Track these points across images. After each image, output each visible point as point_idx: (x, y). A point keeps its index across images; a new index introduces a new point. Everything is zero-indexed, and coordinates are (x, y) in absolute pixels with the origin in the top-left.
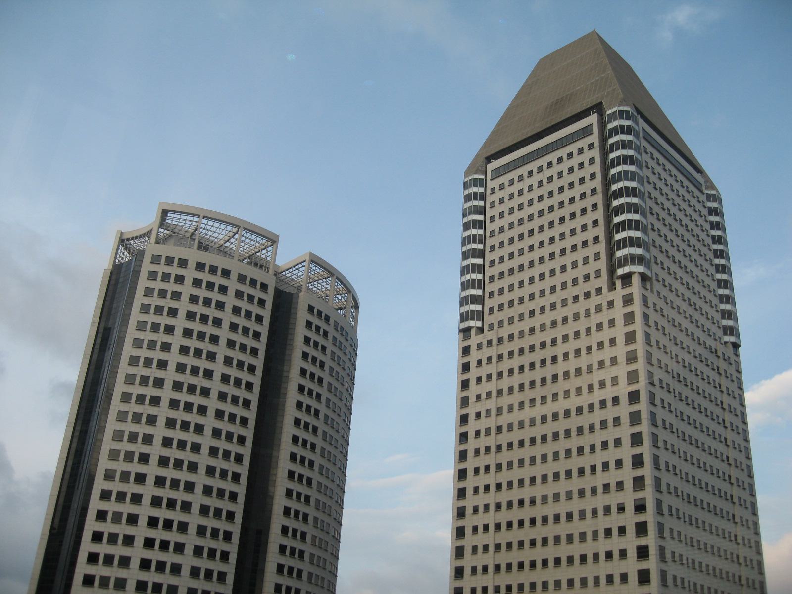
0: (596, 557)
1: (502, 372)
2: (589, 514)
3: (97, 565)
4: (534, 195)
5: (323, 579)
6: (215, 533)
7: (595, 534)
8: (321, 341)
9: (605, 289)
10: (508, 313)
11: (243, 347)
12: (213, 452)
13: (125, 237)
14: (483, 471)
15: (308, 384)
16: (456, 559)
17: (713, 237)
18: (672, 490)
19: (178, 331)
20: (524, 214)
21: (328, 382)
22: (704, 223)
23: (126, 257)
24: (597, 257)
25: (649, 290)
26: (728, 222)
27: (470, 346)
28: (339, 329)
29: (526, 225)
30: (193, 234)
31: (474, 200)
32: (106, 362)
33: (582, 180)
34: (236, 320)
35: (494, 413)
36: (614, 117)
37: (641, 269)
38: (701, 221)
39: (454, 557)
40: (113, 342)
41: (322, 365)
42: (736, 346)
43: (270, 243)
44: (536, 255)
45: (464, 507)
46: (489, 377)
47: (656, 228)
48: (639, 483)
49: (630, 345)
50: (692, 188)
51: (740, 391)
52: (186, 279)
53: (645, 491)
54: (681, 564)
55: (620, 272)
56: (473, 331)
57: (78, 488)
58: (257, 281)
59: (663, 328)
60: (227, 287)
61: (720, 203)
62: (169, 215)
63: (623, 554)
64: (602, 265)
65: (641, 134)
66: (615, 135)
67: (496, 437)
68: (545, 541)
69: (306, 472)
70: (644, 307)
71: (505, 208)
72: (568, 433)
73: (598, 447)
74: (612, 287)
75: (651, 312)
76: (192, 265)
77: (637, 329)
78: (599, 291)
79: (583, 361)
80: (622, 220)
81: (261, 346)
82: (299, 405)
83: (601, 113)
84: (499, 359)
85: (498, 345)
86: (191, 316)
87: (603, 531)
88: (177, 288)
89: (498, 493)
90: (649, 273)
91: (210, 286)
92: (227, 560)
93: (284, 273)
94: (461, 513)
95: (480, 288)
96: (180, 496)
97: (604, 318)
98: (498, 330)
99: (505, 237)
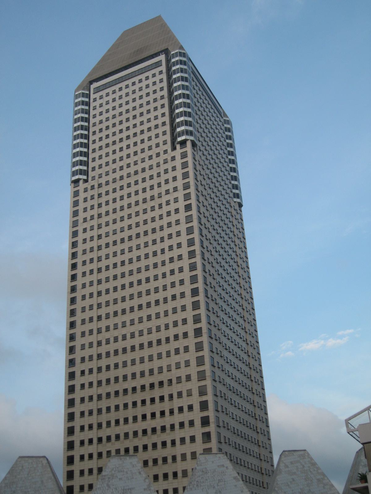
4: (124, 153)
9: (169, 150)
16: (67, 480)
25: (196, 152)
35: (95, 332)
37: (192, 138)
42: (240, 205)
49: (199, 338)
51: (254, 321)
53: (190, 189)
54: (219, 342)
55: (179, 139)
56: (81, 182)
64: (168, 137)
70: (207, 311)
74: (174, 148)
77: (204, 341)
78: (165, 152)
79: (168, 420)
95: (86, 157)
98: (98, 180)
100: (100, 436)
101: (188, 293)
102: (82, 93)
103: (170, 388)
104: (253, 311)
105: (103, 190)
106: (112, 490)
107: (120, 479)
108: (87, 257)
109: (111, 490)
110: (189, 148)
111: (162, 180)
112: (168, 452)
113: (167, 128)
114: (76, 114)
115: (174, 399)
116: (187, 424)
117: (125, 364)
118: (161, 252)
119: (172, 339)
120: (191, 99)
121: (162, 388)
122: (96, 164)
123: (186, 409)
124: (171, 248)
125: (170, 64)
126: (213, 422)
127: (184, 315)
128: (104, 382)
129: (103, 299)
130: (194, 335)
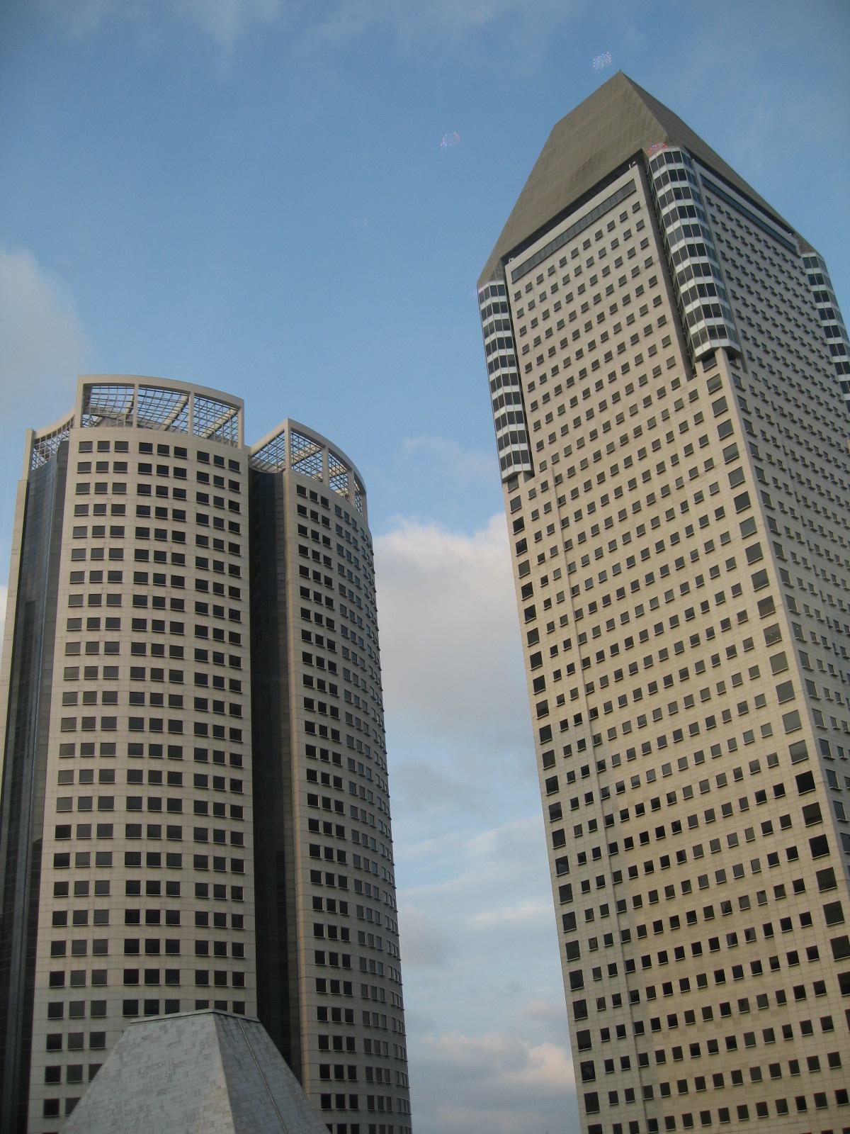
0: (781, 997)
1: (588, 658)
2: (748, 870)
3: (59, 1084)
5: (388, 1071)
6: (220, 949)
7: (756, 865)
8: (327, 656)
9: (683, 379)
11: (218, 658)
12: (200, 835)
13: (39, 436)
14: (584, 803)
15: (318, 719)
17: (827, 329)
19: (122, 750)
20: (564, 314)
21: (344, 669)
22: (839, 406)
23: (40, 460)
25: (741, 370)
26: (839, 290)
27: (540, 653)
28: (348, 615)
30: (128, 416)
31: (510, 423)
32: (20, 890)
34: (203, 621)
36: (659, 162)
37: (725, 342)
39: (573, 1018)
40: (34, 703)
41: (334, 689)
43: (232, 412)
45: (546, 701)
46: (574, 694)
47: (754, 357)
49: (757, 564)
50: (780, 249)
52: (127, 508)
53: (782, 643)
55: (699, 351)
56: (521, 478)
57: (28, 756)
58: (223, 459)
59: (811, 586)
60: (181, 648)
61: (824, 267)
62: (94, 391)
63: (799, 886)
64: (675, 350)
66: (684, 260)
67: (590, 725)
68: (686, 886)
69: (334, 819)
71: (546, 368)
72: (694, 729)
73: (723, 657)
74: (692, 374)
75: (759, 442)
76: (134, 447)
79: (715, 707)
81: (245, 725)
82: (309, 727)
83: (639, 158)
85: (556, 486)
86: (142, 511)
87: (792, 991)
88: (111, 661)
89: (609, 830)
90: (737, 348)
91: (160, 579)
92: (242, 870)
93: (257, 456)
94: (562, 866)
95: (516, 384)
96: (164, 875)
97: (687, 415)
99: (543, 349)
102: (491, 287)
103: (764, 910)
105: (565, 490)
110: (722, 365)
113: (671, 329)
114: (486, 336)
117: (625, 618)
119: (734, 712)
120: (689, 176)
121: (693, 621)
122: (526, 322)
126: (820, 783)
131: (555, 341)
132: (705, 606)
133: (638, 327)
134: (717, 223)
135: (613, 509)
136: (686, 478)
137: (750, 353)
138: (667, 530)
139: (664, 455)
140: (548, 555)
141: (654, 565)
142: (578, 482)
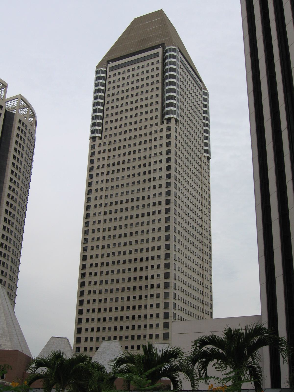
1: (110, 156)
4: (130, 80)
7: (146, 306)
10: (114, 131)
17: (204, 105)
18: (180, 270)
20: (125, 88)
22: (201, 104)
24: (157, 110)
25: (178, 126)
29: (125, 93)
33: (152, 76)
38: (200, 115)
42: (209, 158)
44: (127, 136)
46: (100, 213)
47: (182, 123)
48: (168, 160)
49: (168, 223)
50: (197, 87)
51: (209, 198)
55: (167, 117)
56: (97, 139)
64: (159, 113)
65: (180, 60)
74: (162, 123)
78: (156, 124)
79: (142, 312)
80: (169, 74)
83: (164, 48)
84: (109, 151)
95: (104, 80)
99: (115, 98)
100: (99, 317)
101: (164, 177)
104: (208, 164)
106: (103, 360)
107: (108, 354)
108: (100, 171)
109: (102, 360)
111: (153, 130)
112: (144, 274)
115: (147, 318)
116: (155, 316)
117: (120, 227)
118: (150, 141)
123: (155, 306)
124: (156, 131)
125: (165, 56)
127: (160, 199)
128: (108, 221)
129: (112, 154)
130: (164, 257)
131: (120, 96)
132: (149, 188)
133: (149, 102)
134: (181, 69)
135: (127, 150)
136: (153, 155)
137: (181, 86)
138: (142, 170)
139: (147, 146)
140: (101, 166)
141: (136, 179)
142: (117, 145)
